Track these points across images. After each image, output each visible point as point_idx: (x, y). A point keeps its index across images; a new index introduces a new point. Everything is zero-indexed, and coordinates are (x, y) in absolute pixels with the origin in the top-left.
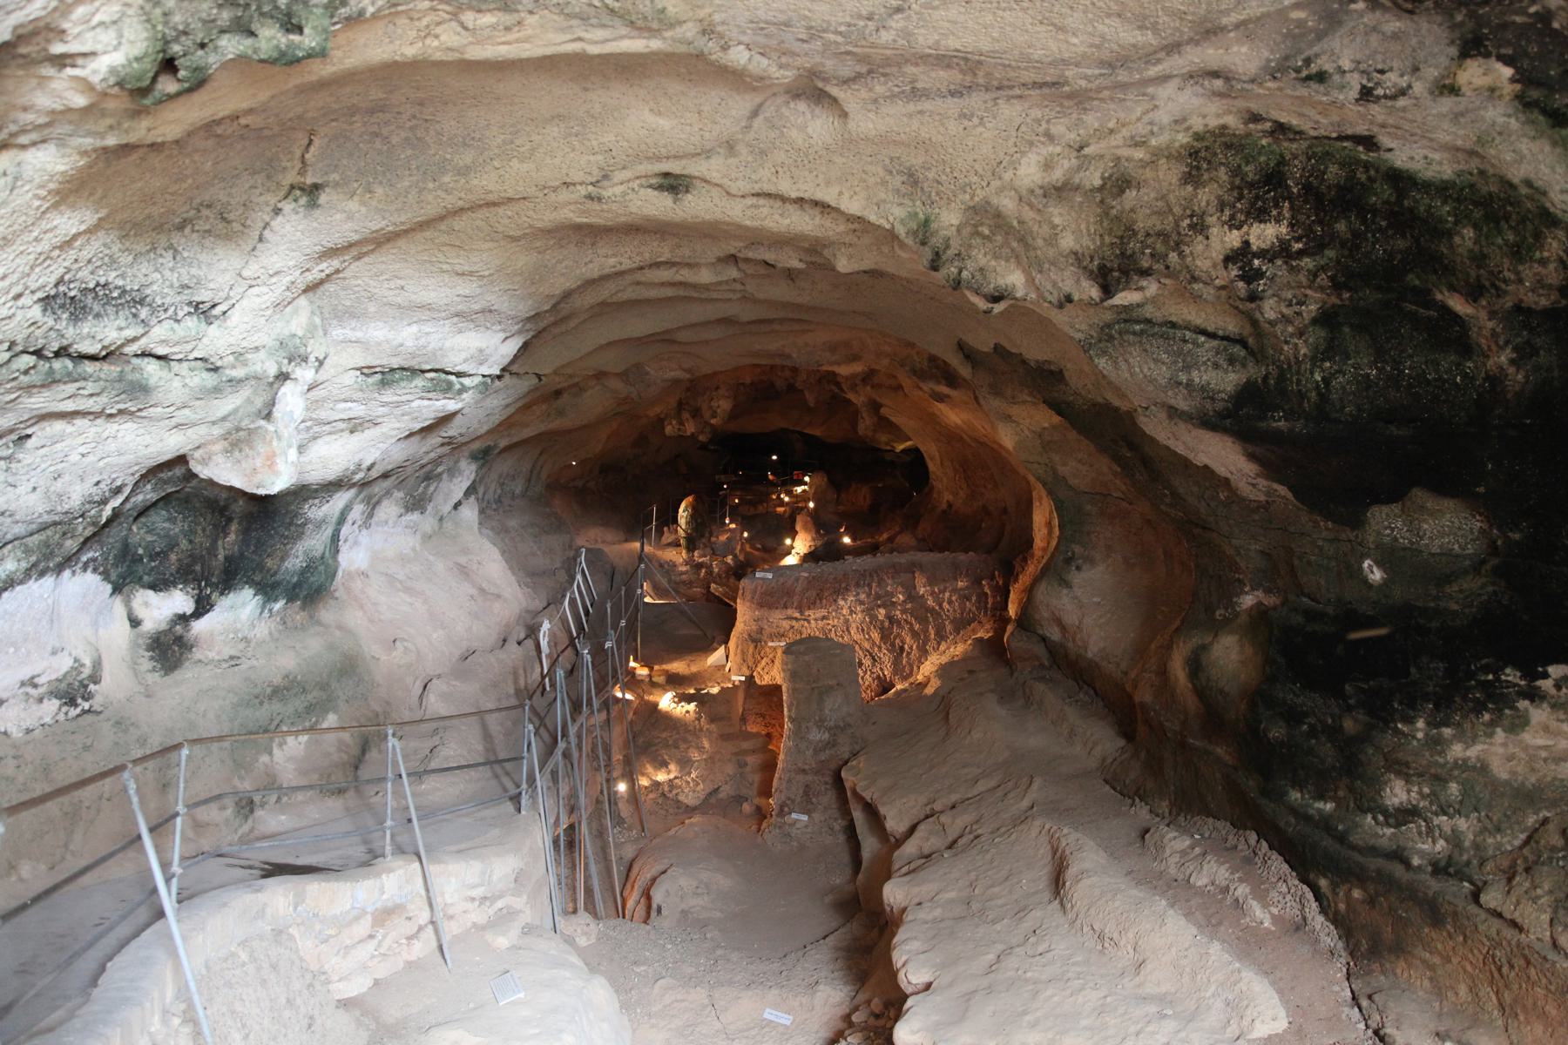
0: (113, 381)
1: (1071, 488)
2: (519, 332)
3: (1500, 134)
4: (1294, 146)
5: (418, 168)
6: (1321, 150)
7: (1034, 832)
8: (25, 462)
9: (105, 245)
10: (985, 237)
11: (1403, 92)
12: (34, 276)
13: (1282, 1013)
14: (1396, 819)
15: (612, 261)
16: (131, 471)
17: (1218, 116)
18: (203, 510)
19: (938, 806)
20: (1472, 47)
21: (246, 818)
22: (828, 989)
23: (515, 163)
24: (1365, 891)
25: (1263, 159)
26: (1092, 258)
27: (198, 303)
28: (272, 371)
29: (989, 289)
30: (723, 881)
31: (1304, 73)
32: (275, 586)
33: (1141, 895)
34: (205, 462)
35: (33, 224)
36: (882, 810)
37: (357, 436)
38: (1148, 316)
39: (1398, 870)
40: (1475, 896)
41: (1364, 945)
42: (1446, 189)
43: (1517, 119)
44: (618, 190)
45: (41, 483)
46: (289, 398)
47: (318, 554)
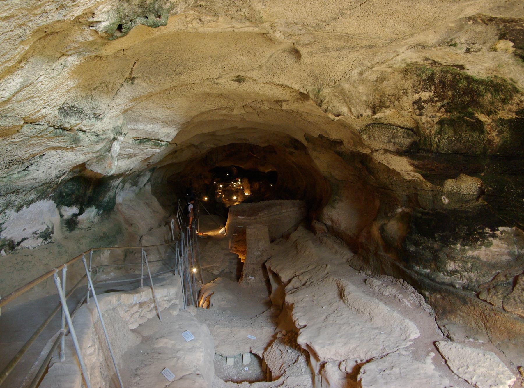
1: (336, 179)
3: (506, 64)
6: (445, 71)
7: (331, 280)
8: (42, 163)
11: (479, 50)
13: (418, 332)
15: (209, 106)
17: (416, 59)
19: (297, 274)
20: (502, 36)
21: (95, 275)
22: (267, 328)
23: (194, 71)
25: (427, 72)
26: (371, 103)
28: (112, 137)
29: (336, 113)
30: (230, 297)
31: (450, 44)
32: (101, 206)
33: (369, 298)
34: (90, 165)
36: (280, 275)
37: (130, 160)
39: (451, 289)
40: (478, 295)
41: (441, 312)
42: (483, 82)
43: (512, 59)
45: (45, 170)
46: (116, 146)
47: (112, 197)
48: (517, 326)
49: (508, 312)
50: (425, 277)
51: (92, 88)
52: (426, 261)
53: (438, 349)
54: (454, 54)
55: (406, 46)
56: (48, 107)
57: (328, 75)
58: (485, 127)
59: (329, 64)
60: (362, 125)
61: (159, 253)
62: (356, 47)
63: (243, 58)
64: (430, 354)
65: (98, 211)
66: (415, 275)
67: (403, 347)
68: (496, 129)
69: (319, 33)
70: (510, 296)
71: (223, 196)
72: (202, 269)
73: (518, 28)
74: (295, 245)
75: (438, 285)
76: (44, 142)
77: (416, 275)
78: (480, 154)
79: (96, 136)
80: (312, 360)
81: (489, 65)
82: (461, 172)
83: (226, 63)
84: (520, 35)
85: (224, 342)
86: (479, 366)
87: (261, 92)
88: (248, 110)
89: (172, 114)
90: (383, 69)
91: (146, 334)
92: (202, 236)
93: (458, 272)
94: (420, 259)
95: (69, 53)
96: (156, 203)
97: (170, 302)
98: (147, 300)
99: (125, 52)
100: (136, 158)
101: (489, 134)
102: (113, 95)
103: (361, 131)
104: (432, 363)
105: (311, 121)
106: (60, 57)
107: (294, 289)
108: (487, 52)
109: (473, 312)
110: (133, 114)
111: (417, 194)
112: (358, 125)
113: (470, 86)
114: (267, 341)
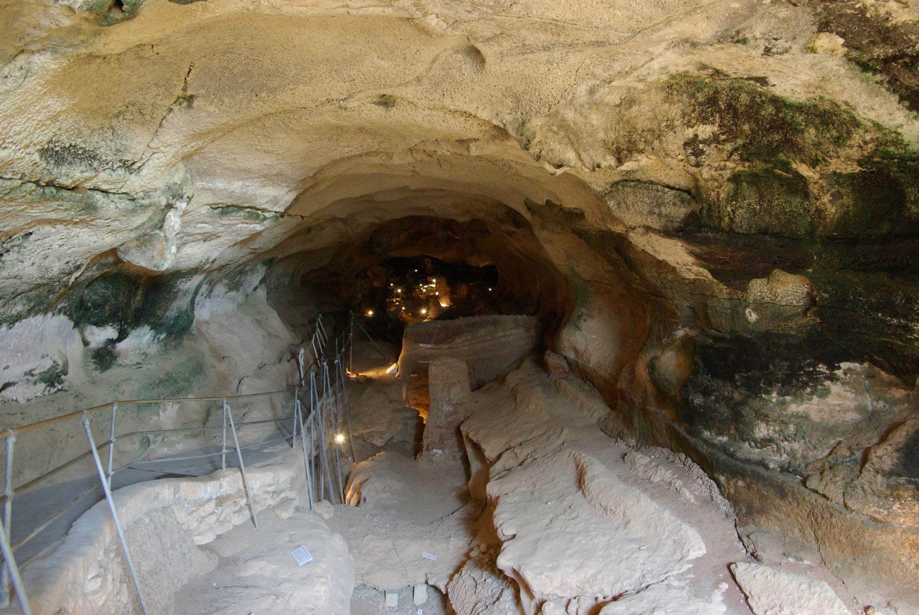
0: (78, 202)
2: (296, 188)
3: (834, 76)
4: (723, 83)
5: (248, 88)
7: (566, 456)
8: (28, 248)
9: (75, 121)
10: (554, 132)
12: (36, 135)
13: (704, 546)
14: (761, 444)
15: (347, 150)
16: (86, 256)
17: (685, 66)
18: (123, 283)
19: (512, 444)
20: (824, 27)
21: (146, 449)
24: (745, 482)
25: (706, 90)
27: (125, 161)
28: (164, 202)
29: (556, 161)
30: (397, 485)
31: (735, 40)
32: (161, 325)
33: (626, 487)
34: (126, 252)
35: (36, 102)
36: (483, 446)
37: (207, 244)
38: (638, 177)
39: (762, 470)
40: (804, 483)
41: (744, 511)
44: (356, 104)
45: (37, 261)
47: (184, 309)
48: (867, 535)
49: (852, 511)
50: (719, 449)
51: (110, 115)
52: (720, 421)
53: (733, 577)
54: (746, 58)
55: (664, 44)
56: (14, 147)
57: (537, 94)
58: (811, 186)
59: (535, 75)
60: (606, 184)
61: (274, 408)
62: (577, 45)
63: (383, 63)
64: (721, 586)
65: (156, 334)
66: (702, 447)
67: (676, 572)
68: (828, 191)
69: (503, 17)
70: (856, 482)
71: (403, 308)
72: (354, 436)
73: (849, 11)
74: (514, 394)
75: (741, 464)
76: (23, 210)
77: (705, 447)
78: (804, 235)
79: (130, 200)
80: (523, 596)
81: (807, 78)
82: (775, 265)
83: (355, 72)
84: (854, 25)
85: (381, 565)
86: (800, 607)
87: (425, 125)
88: (419, 156)
89: (276, 162)
90: (630, 85)
91: (227, 552)
92: (356, 378)
93: (773, 442)
94: (712, 419)
95: (33, 47)
96: (275, 321)
97: (278, 496)
98: (232, 492)
99: (155, 49)
100: (219, 240)
101: (817, 199)
102: (155, 128)
103: (606, 194)
104: (723, 601)
105: (529, 176)
106: (16, 55)
107: (505, 470)
108: (800, 54)
109: (796, 511)
110: (202, 161)
111: (706, 306)
112: (599, 182)
113: (780, 115)
114: (455, 563)
